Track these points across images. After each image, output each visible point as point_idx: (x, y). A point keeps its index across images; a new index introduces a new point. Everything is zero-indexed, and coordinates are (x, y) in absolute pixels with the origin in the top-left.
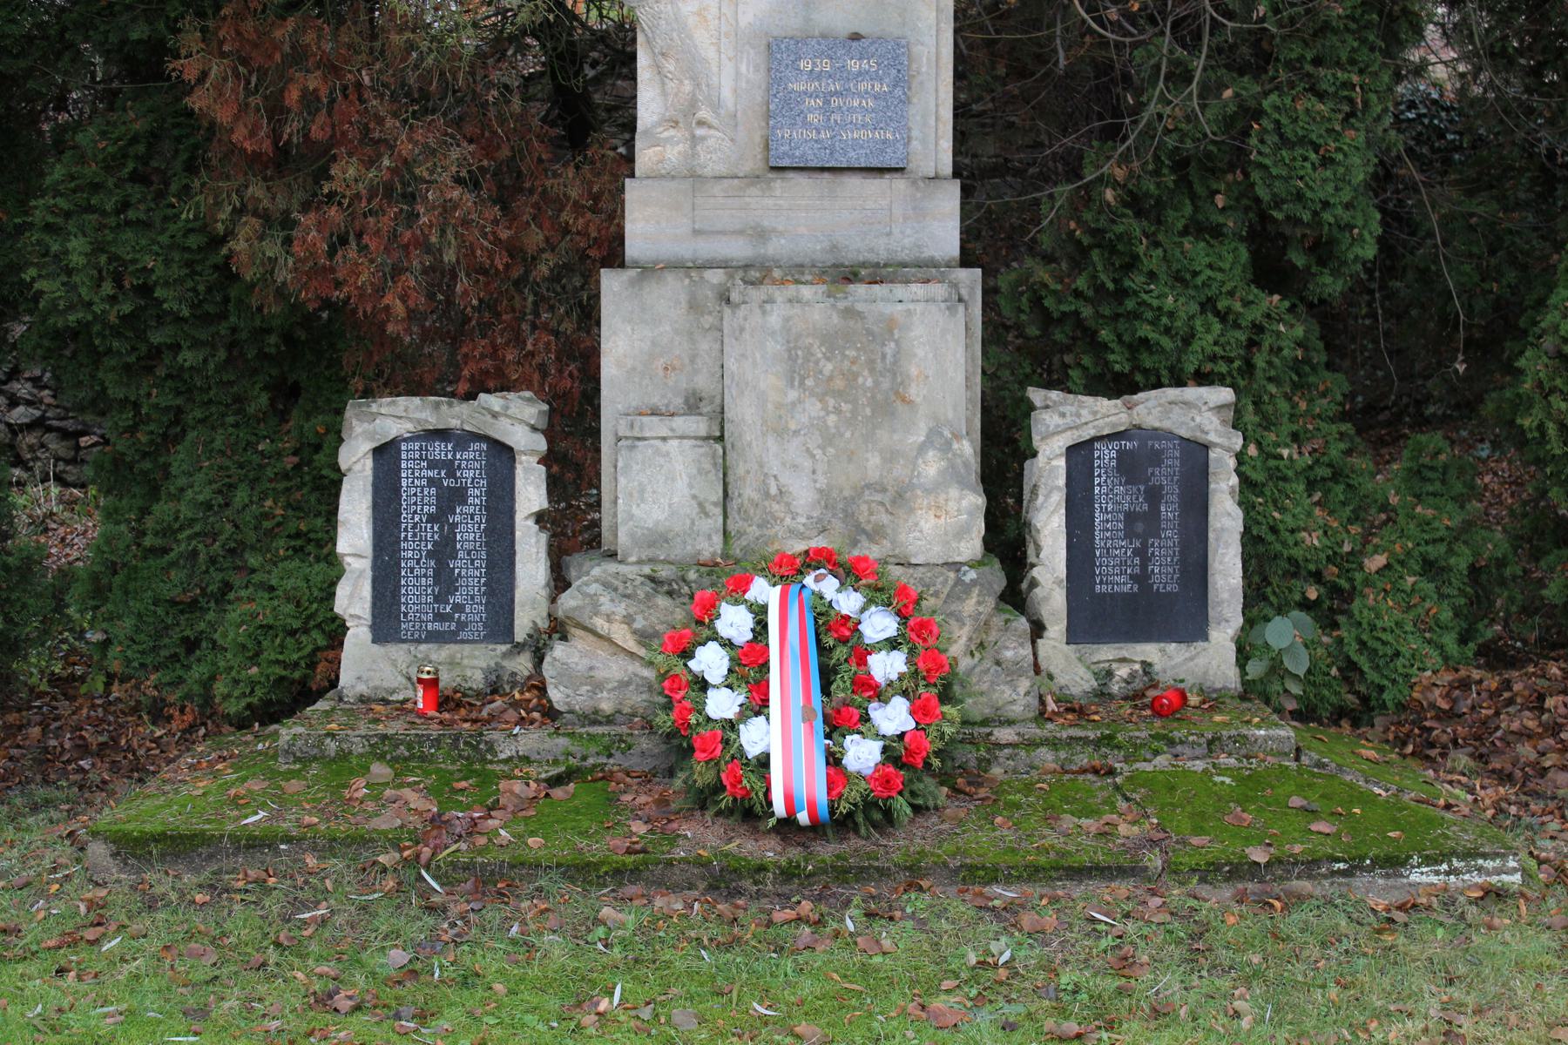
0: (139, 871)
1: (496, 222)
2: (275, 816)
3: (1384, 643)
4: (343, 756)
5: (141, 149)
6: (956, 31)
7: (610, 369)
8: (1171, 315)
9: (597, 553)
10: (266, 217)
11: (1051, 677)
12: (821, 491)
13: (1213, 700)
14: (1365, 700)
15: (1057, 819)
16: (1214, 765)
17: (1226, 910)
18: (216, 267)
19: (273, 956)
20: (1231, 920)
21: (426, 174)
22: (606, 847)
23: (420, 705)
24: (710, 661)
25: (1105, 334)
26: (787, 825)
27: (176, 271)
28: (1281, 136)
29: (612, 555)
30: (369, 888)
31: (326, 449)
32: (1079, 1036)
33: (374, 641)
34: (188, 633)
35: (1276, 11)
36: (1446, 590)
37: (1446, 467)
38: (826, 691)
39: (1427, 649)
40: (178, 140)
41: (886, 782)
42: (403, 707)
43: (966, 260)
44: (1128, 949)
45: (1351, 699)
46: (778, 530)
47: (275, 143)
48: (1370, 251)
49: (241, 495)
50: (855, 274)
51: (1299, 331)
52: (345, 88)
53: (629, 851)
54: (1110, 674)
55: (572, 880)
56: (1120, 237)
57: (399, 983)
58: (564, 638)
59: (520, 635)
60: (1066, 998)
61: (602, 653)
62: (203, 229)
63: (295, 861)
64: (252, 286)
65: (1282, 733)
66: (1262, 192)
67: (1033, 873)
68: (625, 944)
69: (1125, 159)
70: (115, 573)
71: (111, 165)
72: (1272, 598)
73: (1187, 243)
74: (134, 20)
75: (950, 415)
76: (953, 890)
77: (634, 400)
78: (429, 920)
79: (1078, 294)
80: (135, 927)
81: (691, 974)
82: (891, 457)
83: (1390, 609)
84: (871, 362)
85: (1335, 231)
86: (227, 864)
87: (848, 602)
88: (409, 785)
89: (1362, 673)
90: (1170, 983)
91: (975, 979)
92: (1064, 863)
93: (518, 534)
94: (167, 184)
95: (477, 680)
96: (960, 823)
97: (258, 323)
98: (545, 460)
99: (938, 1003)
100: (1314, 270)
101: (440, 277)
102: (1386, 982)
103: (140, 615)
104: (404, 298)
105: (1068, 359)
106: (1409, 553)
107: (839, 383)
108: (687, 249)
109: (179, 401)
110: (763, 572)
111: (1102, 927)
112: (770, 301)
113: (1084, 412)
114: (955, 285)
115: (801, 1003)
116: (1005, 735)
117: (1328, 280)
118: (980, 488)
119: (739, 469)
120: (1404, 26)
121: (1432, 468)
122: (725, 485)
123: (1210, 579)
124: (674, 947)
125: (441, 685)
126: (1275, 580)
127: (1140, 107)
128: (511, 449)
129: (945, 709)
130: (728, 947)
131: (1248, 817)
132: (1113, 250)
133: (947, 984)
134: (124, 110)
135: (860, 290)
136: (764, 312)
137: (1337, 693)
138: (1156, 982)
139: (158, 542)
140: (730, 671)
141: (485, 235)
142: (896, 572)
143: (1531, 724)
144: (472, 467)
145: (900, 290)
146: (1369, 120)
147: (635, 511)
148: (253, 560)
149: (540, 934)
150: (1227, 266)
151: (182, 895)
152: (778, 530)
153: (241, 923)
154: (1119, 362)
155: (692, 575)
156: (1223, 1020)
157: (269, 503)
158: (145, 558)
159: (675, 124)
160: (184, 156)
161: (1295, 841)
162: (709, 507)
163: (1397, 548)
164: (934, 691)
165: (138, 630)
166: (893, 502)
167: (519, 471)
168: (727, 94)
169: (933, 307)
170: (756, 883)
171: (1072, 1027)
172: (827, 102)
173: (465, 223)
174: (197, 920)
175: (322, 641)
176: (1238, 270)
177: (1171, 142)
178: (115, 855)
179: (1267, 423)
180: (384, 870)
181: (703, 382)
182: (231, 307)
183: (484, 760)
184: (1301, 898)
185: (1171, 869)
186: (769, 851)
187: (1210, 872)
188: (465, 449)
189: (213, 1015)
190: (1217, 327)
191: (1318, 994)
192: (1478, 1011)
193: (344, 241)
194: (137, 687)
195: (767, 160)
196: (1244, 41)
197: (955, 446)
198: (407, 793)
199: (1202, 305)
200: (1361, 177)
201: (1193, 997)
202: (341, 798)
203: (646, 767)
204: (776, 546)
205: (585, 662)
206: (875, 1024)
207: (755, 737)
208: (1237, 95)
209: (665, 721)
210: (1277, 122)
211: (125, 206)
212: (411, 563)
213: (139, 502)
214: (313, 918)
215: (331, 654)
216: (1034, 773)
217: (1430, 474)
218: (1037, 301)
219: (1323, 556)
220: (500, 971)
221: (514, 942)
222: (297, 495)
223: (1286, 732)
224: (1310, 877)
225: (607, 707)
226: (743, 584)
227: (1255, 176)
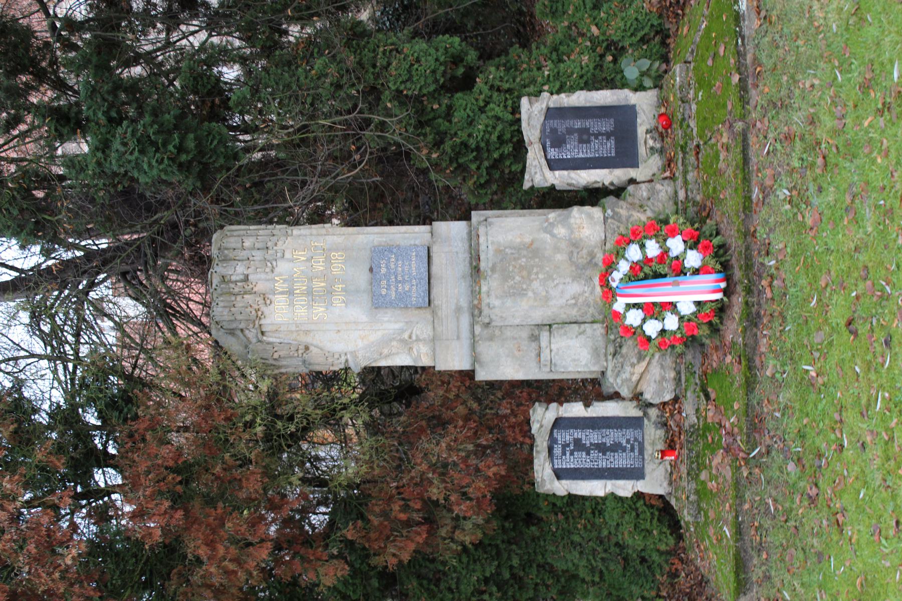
0: (752, 583)
1: (455, 427)
2: (726, 522)
3: (632, 25)
4: (697, 492)
5: (425, 582)
6: (366, 225)
7: (520, 376)
8: (487, 126)
10: (455, 528)
11: (654, 175)
12: (573, 280)
13: (663, 101)
14: (657, 33)
15: (721, 170)
16: (694, 100)
17: (762, 92)
18: (476, 550)
19: (792, 523)
20: (767, 90)
21: (436, 458)
22: (738, 375)
23: (673, 458)
24: (652, 328)
26: (726, 292)
27: (478, 567)
28: (407, 81)
29: (603, 373)
31: (554, 501)
32: (824, 158)
33: (644, 478)
35: (354, 85)
38: (665, 276)
40: (421, 566)
41: (706, 248)
42: (674, 466)
43: (467, 217)
44: (781, 136)
45: (658, 39)
46: (591, 300)
47: (422, 524)
48: (457, 40)
49: (576, 538)
50: (475, 267)
51: (493, 69)
52: (399, 493)
53: (740, 363)
54: (652, 148)
55: (753, 389)
56: (453, 150)
57: (803, 466)
58: (641, 394)
59: (639, 414)
60: (805, 164)
61: (648, 377)
62: (459, 555)
63: (747, 513)
64: (484, 533)
65: (678, 70)
66: (432, 88)
67: (746, 180)
68: (783, 365)
69: (419, 149)
70: (611, 594)
72: (612, 76)
74: (370, 585)
75: (537, 223)
76: (755, 216)
77: (533, 364)
78: (774, 453)
79: (478, 168)
80: (779, 585)
81: (797, 334)
84: (515, 259)
85: (448, 55)
86: (748, 544)
87: (624, 267)
88: (710, 462)
89: (645, 35)
91: (797, 206)
92: (741, 166)
93: (594, 415)
94: (439, 571)
95: (660, 433)
96: (723, 214)
97: (500, 531)
98: (561, 404)
99: (809, 222)
100: (465, 64)
101: (481, 451)
102: (794, 19)
103: (630, 583)
104: (489, 468)
105: (507, 171)
107: (525, 273)
108: (466, 342)
109: (535, 565)
110: (611, 306)
111: (771, 149)
112: (488, 305)
113: (534, 163)
114: (479, 223)
115: (810, 284)
116: (682, 195)
117: (469, 57)
118: (570, 209)
119: (563, 317)
120: (358, 29)
121: (552, 7)
122: (571, 323)
123: (608, 104)
124: (785, 342)
125: (663, 449)
126: (604, 75)
127: (398, 145)
128: (556, 419)
129: (671, 222)
130: (784, 319)
131: (718, 84)
132: (459, 153)
133: (800, 218)
134: (408, 589)
135: (483, 265)
136: (494, 307)
137: (655, 45)
138: (797, 123)
140: (656, 319)
141: (461, 432)
142: (609, 246)
144: (565, 436)
145: (483, 247)
146: (399, 42)
147: (583, 363)
148: (605, 533)
150: (465, 103)
151: (763, 564)
152: (591, 300)
153: (776, 538)
154: (508, 149)
155: (612, 337)
156: (815, 92)
157: (579, 526)
158: (605, 581)
159: (411, 349)
160: (428, 564)
161: (728, 63)
162: (581, 330)
163: (588, 21)
164: (663, 227)
165: (637, 584)
166: (577, 248)
168: (397, 326)
169: (490, 233)
170: (753, 306)
171: (820, 161)
172: (400, 282)
174: (774, 558)
175: (642, 502)
176: (466, 97)
177: (411, 130)
178: (745, 594)
179: (533, 81)
180: (750, 473)
181: (525, 334)
182: (493, 543)
183: (698, 429)
184: (755, 59)
185: (743, 118)
186: (738, 300)
187: (744, 100)
189: (821, 550)
190: (492, 105)
191: (802, 50)
193: (464, 494)
194: (662, 584)
195: (426, 308)
196: (366, 99)
197: (551, 220)
198: (714, 464)
199: (482, 113)
200: (424, 45)
201: (804, 106)
202: (717, 493)
204: (598, 299)
205: (652, 384)
206: (820, 250)
207: (687, 307)
208: (390, 101)
209: (679, 348)
210: (401, 83)
211: (450, 590)
212: (608, 462)
213: (579, 583)
214: (773, 505)
215: (647, 498)
216: (699, 181)
217: (554, 8)
218: (482, 186)
219: (592, 54)
220: (797, 420)
221: (783, 415)
222: (575, 513)
223: (677, 68)
224: (745, 55)
225: (672, 374)
226: (616, 315)
227: (425, 91)
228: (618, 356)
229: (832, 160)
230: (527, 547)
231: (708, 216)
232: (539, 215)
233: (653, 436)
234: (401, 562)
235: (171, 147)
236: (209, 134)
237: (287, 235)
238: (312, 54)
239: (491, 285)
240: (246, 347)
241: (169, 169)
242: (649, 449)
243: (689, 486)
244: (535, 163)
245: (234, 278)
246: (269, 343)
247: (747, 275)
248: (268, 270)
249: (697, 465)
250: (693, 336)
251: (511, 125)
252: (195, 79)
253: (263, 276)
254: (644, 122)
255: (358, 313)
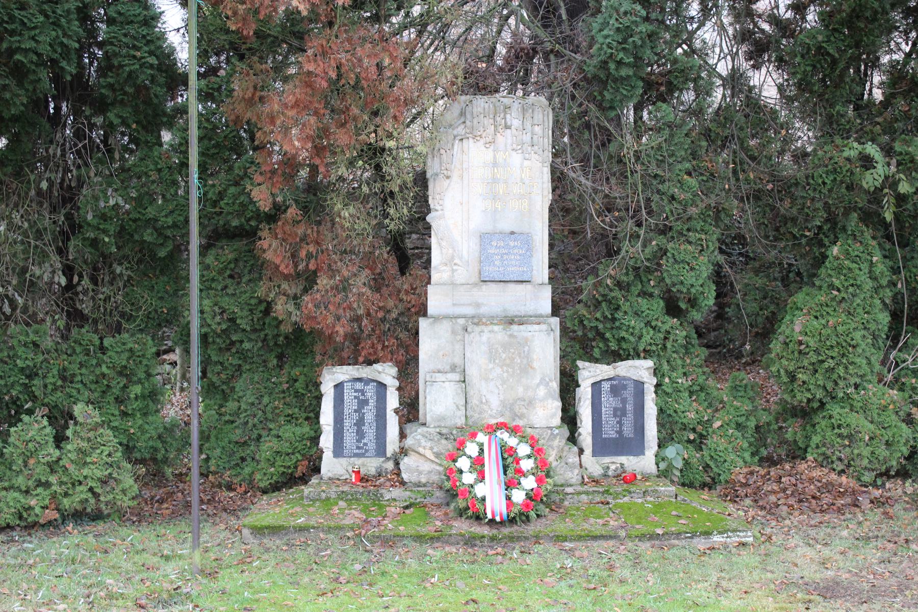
4: (328, 499)
8: (633, 328)
9: (416, 424)
13: (646, 478)
14: (713, 479)
22: (424, 530)
24: (463, 463)
25: (608, 335)
26: (492, 522)
27: (246, 313)
29: (424, 424)
30: (344, 545)
34: (243, 455)
36: (746, 435)
37: (746, 386)
39: (738, 459)
41: (527, 506)
43: (555, 311)
44: (612, 563)
45: (708, 480)
48: (711, 302)
49: (266, 400)
51: (684, 333)
53: (436, 531)
54: (608, 468)
55: (415, 541)
56: (613, 298)
67: (580, 538)
71: (221, 272)
73: (640, 299)
77: (432, 367)
78: (367, 555)
79: (597, 319)
80: (264, 557)
82: (527, 388)
83: (722, 444)
86: (291, 536)
87: (512, 441)
90: (626, 573)
93: (388, 417)
95: (373, 471)
103: (223, 448)
105: (594, 344)
106: (730, 420)
107: (508, 361)
108: (450, 311)
114: (549, 325)
116: (569, 490)
117: (695, 313)
119: (471, 392)
126: (676, 432)
130: (473, 563)
131: (657, 518)
132: (611, 303)
133: (549, 574)
135: (515, 327)
139: (231, 418)
143: (775, 488)
144: (371, 392)
145: (530, 327)
149: (407, 559)
150: (654, 309)
151: (277, 547)
152: (486, 415)
153: (301, 556)
154: (613, 346)
155: (454, 432)
157: (277, 403)
160: (249, 268)
163: (726, 418)
164: (543, 473)
167: (388, 393)
168: (465, 253)
171: (593, 586)
173: (368, 300)
174: (285, 555)
176: (660, 309)
179: (673, 369)
180: (349, 538)
181: (458, 360)
183: (379, 500)
184: (674, 546)
186: (486, 531)
187: (642, 537)
188: (368, 385)
190: (652, 332)
192: (730, 579)
194: (221, 477)
198: (353, 511)
203: (438, 502)
205: (416, 464)
207: (480, 490)
208: (658, 245)
209: (448, 485)
211: (226, 287)
218: (581, 322)
223: (672, 489)
225: (423, 480)
226: (474, 435)
227: (665, 275)
228: (439, 436)
229: (593, 593)
230: (259, 355)
231: (552, 510)
232: (555, 374)
233: (370, 465)
234: (264, 251)
235: (621, 55)
236: (633, 87)
237: (543, 162)
238: (702, 174)
239: (498, 333)
240: (451, 126)
241: (602, 53)
242: (358, 462)
243: (333, 492)
244: (598, 372)
245: (508, 116)
246: (453, 145)
247: (505, 538)
248: (515, 146)
249: (352, 499)
250: (457, 495)
251: (634, 349)
252: (683, 71)
253: (509, 141)
254: (630, 463)
255: (478, 221)
